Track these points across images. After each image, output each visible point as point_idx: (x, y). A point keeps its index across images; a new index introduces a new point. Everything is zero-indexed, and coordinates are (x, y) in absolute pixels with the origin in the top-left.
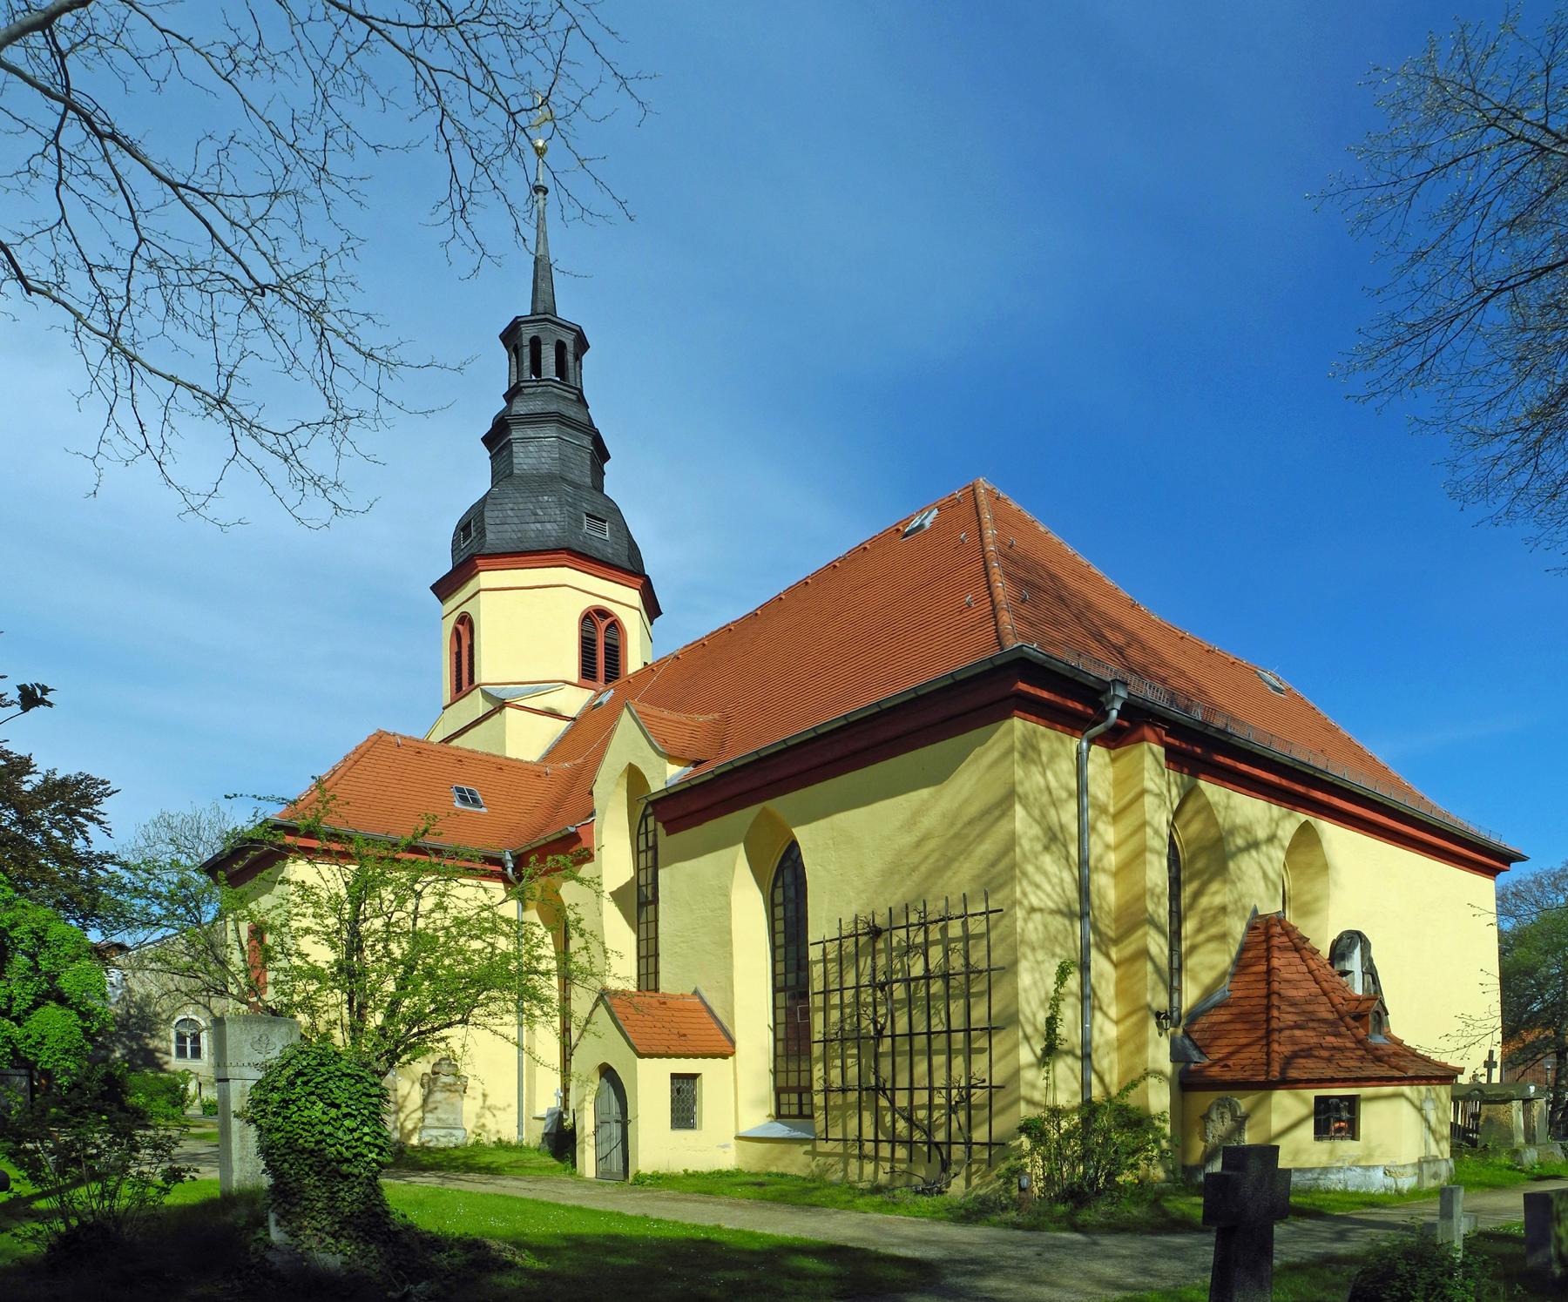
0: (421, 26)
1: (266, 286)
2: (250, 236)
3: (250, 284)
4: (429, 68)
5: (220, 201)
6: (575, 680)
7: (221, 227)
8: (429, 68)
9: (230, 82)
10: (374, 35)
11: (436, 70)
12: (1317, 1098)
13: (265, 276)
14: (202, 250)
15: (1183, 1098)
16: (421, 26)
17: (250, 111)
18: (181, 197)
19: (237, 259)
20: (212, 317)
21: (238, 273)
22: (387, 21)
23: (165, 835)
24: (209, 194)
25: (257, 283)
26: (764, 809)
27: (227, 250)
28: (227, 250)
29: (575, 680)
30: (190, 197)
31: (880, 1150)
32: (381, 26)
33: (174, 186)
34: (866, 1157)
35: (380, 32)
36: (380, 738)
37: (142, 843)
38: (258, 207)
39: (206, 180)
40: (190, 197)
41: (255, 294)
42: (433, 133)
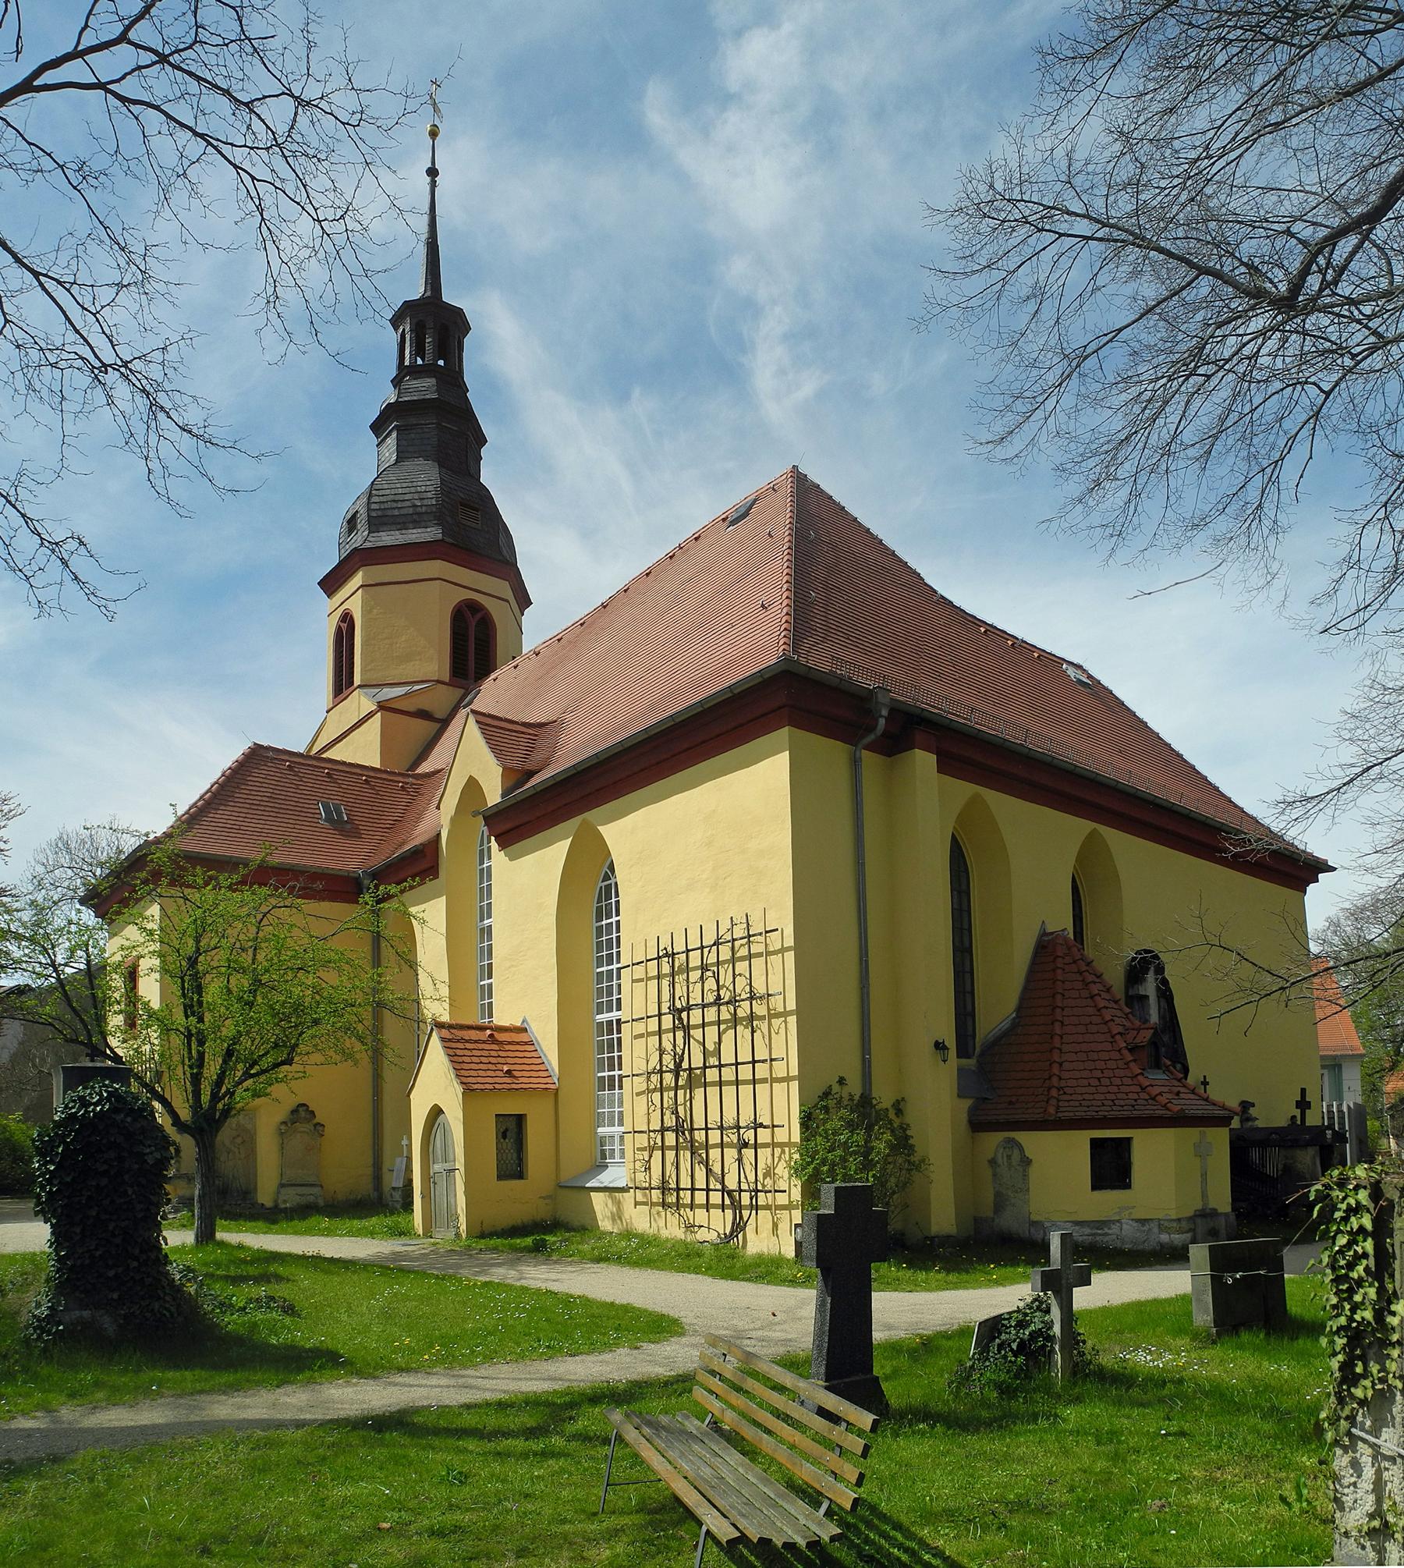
0: (58, 164)
1: (110, 366)
2: (98, 320)
3: (97, 364)
4: (253, 178)
5: (75, 289)
6: (447, 680)
7: (75, 313)
8: (253, 178)
9: (79, 191)
10: (210, 149)
11: (258, 180)
12: (1042, 1271)
13: (108, 357)
14: (58, 332)
15: (972, 1138)
16: (58, 164)
17: (93, 216)
18: (41, 285)
19: (85, 340)
20: (61, 391)
21: (86, 352)
22: (218, 140)
23: (65, 860)
24: (64, 282)
25: (101, 361)
26: (584, 820)
27: (77, 332)
28: (77, 332)
29: (447, 680)
30: (50, 285)
31: (711, 1199)
32: (215, 143)
33: (36, 275)
34: (761, 1125)
35: (215, 147)
36: (257, 756)
37: (41, 869)
38: (105, 295)
39: (66, 271)
40: (50, 285)
41: (100, 372)
42: (255, 232)
